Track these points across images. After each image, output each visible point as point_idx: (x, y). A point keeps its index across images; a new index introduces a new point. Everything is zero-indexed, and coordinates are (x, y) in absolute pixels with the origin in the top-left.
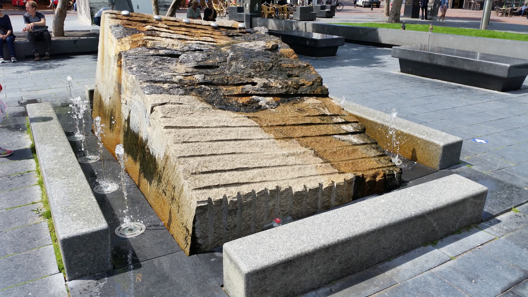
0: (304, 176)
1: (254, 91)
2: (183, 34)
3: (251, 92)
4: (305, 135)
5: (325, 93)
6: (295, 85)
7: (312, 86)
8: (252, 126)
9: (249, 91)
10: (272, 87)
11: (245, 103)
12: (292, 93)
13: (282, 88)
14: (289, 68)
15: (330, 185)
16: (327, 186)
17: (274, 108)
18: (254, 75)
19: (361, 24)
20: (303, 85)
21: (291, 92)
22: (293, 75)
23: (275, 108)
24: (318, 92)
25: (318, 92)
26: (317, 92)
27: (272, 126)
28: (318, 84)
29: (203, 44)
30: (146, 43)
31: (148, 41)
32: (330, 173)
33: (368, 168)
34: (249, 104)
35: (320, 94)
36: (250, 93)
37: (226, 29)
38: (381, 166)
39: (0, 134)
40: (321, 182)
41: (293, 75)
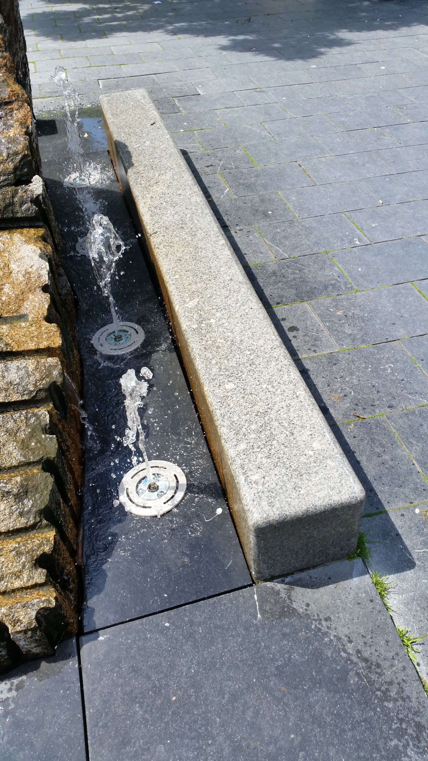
5: (19, 215)
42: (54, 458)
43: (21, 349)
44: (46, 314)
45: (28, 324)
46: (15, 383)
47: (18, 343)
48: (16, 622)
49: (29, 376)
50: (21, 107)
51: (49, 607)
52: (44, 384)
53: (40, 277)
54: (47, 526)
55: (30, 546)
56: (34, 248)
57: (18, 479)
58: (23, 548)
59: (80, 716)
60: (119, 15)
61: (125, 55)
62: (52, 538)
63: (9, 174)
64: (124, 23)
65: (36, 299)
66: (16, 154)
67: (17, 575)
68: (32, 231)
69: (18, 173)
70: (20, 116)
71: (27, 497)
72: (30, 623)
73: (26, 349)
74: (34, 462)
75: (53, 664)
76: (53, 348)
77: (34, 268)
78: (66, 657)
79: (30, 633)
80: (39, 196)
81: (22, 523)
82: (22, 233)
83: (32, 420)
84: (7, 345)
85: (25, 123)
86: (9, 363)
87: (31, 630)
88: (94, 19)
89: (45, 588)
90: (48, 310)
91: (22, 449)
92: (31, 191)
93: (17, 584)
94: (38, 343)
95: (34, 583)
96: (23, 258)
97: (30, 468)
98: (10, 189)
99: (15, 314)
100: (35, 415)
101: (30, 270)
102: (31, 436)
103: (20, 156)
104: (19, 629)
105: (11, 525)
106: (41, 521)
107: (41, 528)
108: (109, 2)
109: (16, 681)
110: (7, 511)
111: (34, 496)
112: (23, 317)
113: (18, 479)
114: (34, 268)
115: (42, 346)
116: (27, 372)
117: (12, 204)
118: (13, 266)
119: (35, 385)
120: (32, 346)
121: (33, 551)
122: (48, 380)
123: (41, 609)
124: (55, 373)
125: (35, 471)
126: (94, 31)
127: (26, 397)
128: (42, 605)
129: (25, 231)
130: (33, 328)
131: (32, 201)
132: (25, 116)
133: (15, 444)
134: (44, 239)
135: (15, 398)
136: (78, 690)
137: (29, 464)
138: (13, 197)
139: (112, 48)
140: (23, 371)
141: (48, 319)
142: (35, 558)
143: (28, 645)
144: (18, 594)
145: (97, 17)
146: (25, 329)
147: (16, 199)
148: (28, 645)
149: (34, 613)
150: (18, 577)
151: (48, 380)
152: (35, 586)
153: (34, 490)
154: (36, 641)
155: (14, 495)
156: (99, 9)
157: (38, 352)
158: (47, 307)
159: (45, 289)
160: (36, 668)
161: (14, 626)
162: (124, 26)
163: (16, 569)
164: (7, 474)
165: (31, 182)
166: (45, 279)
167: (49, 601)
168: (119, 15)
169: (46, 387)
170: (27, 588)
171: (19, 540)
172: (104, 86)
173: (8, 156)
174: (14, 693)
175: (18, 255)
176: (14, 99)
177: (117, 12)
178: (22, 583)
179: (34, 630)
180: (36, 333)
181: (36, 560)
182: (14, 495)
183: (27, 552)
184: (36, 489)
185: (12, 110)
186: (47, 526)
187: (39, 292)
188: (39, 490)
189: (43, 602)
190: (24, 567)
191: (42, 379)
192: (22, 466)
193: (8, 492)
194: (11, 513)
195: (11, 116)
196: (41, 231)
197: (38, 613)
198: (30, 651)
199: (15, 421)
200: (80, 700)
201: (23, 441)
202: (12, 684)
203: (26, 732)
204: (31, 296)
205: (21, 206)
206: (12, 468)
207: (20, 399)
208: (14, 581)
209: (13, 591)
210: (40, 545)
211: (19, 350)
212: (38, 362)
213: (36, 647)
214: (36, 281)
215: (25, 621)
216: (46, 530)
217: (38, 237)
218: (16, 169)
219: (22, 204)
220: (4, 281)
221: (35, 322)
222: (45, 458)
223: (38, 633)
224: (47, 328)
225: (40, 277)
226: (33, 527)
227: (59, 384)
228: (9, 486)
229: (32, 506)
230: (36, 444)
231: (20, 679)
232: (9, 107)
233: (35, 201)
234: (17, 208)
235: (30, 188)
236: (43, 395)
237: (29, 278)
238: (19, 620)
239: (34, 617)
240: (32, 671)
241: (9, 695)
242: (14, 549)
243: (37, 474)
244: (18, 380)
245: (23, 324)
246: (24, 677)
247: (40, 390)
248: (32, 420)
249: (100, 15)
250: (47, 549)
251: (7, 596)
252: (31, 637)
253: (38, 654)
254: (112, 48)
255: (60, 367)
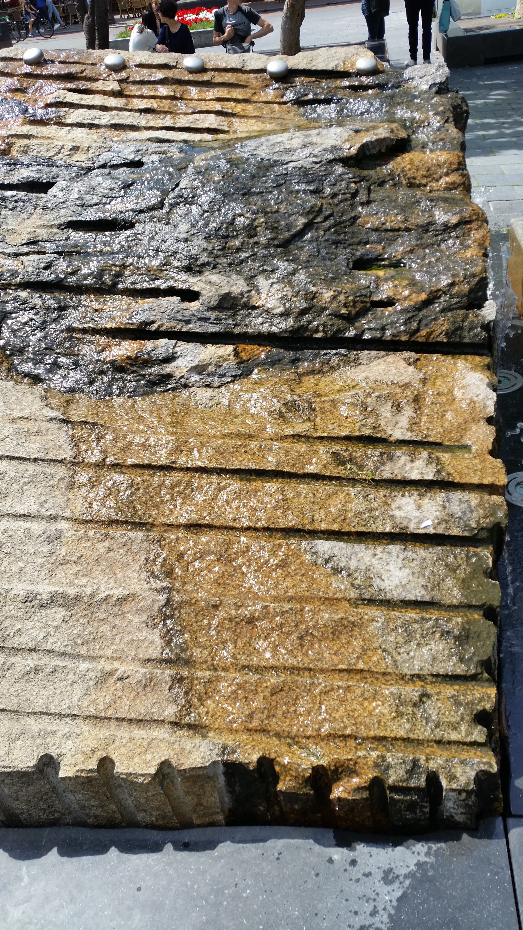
0: (15, 708)
1: (173, 323)
2: (141, 111)
3: (160, 327)
4: (200, 522)
5: (466, 340)
6: (345, 305)
7: (420, 309)
8: (42, 460)
9: (153, 322)
10: (254, 308)
11: (118, 363)
12: (319, 335)
13: (285, 314)
14: (386, 230)
15: (84, 775)
16: (71, 774)
17: (216, 384)
18: (208, 263)
19: (480, 78)
20: (389, 303)
21: (317, 331)
22: (384, 260)
23: (219, 387)
24: (436, 333)
25: (436, 333)
26: (430, 334)
27: (118, 465)
28: (455, 300)
29: (168, 141)
30: (10, 146)
31: (14, 140)
32: (133, 716)
33: (325, 729)
34: (132, 365)
35: (442, 343)
36: (154, 327)
37: (314, 79)
38: (402, 733)
39: (522, 192)
40: (58, 751)
41: (384, 260)
42: (497, 607)
43: (463, 481)
44: (490, 447)
45: (471, 456)
46: (457, 516)
47: (460, 473)
48: (452, 778)
49: (472, 511)
50: (480, 227)
51: (490, 772)
52: (486, 522)
53: (485, 407)
54: (487, 680)
55: (470, 698)
56: (482, 376)
57: (459, 620)
58: (462, 697)
59: (513, 909)
60: (508, 131)
61: (519, 175)
62: (493, 696)
63: (464, 296)
64: (514, 139)
65: (480, 431)
66: (473, 276)
67: (455, 727)
68: (478, 359)
69: (472, 296)
70: (478, 236)
71: (467, 643)
72: (468, 784)
73: (468, 482)
74: (475, 606)
75: (477, 840)
76: (497, 485)
77: (481, 397)
78: (489, 835)
79: (464, 795)
80: (490, 322)
81: (461, 669)
82: (466, 360)
83: (474, 560)
84: (449, 474)
85: (483, 244)
86: (451, 493)
87: (467, 791)
88: (479, 137)
89: (484, 749)
90: (493, 443)
91: (463, 589)
92: (483, 316)
93: (454, 736)
94: (482, 478)
95: (472, 740)
96: (469, 385)
97: (470, 611)
98: (461, 312)
99: (456, 444)
100: (476, 554)
101: (476, 399)
102: (472, 576)
103: (477, 279)
104: (454, 786)
105: (450, 669)
106: (482, 673)
107: (481, 680)
108: (495, 117)
109: (434, 846)
110: (446, 652)
111: (476, 642)
112: (466, 448)
113: (459, 620)
114: (481, 397)
115: (486, 482)
116: (470, 506)
117: (461, 328)
118: (458, 393)
119: (478, 522)
120: (475, 480)
121: (473, 704)
122: (492, 519)
123: (482, 771)
124: (500, 514)
125: (476, 616)
126: (479, 148)
127: (466, 534)
128: (483, 767)
129: (470, 357)
130: (477, 461)
131: (481, 327)
132: (483, 236)
133: (455, 581)
134: (488, 367)
135: (455, 532)
136: (508, 878)
137: (470, 607)
138: (463, 321)
139: (501, 166)
140: (466, 505)
141: (493, 453)
142: (475, 712)
143: (454, 809)
144: (454, 748)
145: (481, 133)
146: (468, 461)
147: (466, 324)
148: (454, 809)
149: (473, 774)
150: (455, 728)
151: (492, 519)
152: (474, 744)
153: (476, 637)
154: (467, 805)
155: (455, 637)
156: (483, 124)
157: (479, 487)
158: (492, 440)
159: (490, 421)
160: (458, 838)
161: (450, 782)
162: (515, 143)
163: (454, 720)
164: (446, 611)
165: (483, 307)
166: (491, 410)
167: (491, 766)
168: (508, 131)
169: (490, 526)
170: (464, 744)
171: (457, 687)
172: (495, 209)
173: (465, 278)
174: (431, 860)
175: (464, 382)
176: (474, 218)
177: (505, 128)
178: (460, 736)
179: (469, 793)
180: (480, 467)
181: (475, 715)
182: (455, 637)
183: (467, 704)
184: (478, 637)
185: (470, 230)
186: (487, 680)
187: (483, 423)
188: (481, 638)
189: (484, 764)
190: (462, 719)
191: (486, 517)
192: (463, 607)
193: (448, 632)
194: (450, 656)
195: (469, 235)
196: (487, 360)
197: (477, 775)
198: (452, 817)
199: (455, 557)
200: (511, 890)
201: (464, 580)
202: (430, 848)
203: (449, 907)
204: (474, 428)
205: (469, 331)
206: (451, 607)
207: (460, 534)
208: (451, 732)
209: (449, 743)
210: (481, 700)
211: (461, 481)
212: (482, 498)
213: (462, 813)
214: (481, 411)
215: (463, 780)
216: (486, 684)
217: (484, 365)
218: (471, 291)
219: (471, 329)
220: (447, 407)
221: (478, 455)
222: (488, 604)
223: (473, 798)
224: (492, 463)
225: (485, 407)
226: (474, 678)
227: (503, 526)
228: (450, 625)
229: (474, 654)
230: (478, 586)
231: (439, 845)
232: (468, 226)
233: (486, 327)
234: (465, 333)
235: (482, 313)
236: (484, 534)
237: (474, 408)
238: (455, 777)
239: (472, 778)
240: (453, 840)
241: (427, 860)
242: (452, 697)
243: (479, 621)
244: (460, 513)
245: (466, 456)
246: (443, 845)
247: (483, 529)
248: (474, 560)
249: (485, 131)
250: (488, 706)
251: (441, 746)
252: (463, 800)
253: (459, 823)
254: (501, 166)
255: (506, 507)
